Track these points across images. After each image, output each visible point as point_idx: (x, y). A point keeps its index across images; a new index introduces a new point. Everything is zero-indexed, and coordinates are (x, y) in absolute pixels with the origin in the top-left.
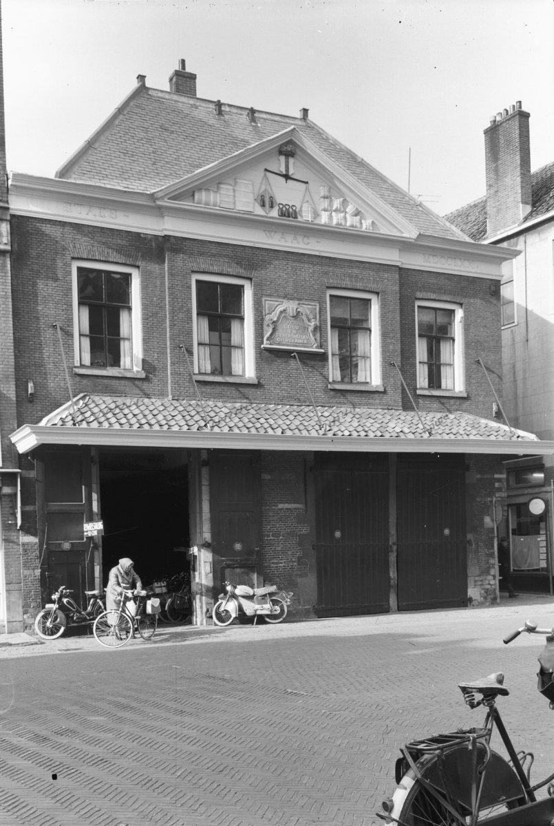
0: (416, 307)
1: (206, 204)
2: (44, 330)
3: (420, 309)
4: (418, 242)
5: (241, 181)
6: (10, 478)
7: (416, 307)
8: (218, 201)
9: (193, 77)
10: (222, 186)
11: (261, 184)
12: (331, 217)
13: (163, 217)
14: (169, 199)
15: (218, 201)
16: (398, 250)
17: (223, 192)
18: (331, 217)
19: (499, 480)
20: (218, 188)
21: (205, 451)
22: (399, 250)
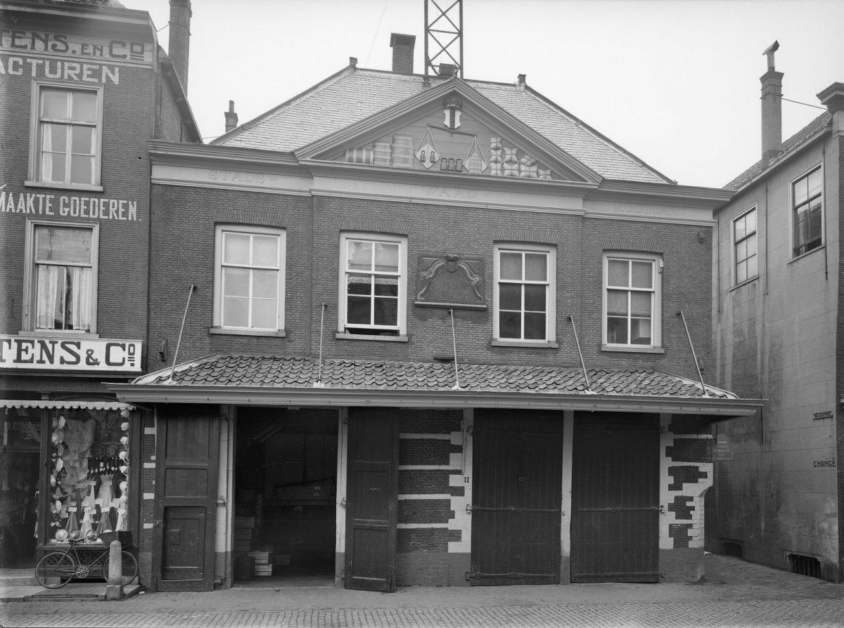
0: (605, 293)
1: (366, 163)
2: (162, 248)
3: (612, 295)
4: (601, 189)
5: (400, 137)
6: (843, 596)
7: (605, 293)
8: (372, 159)
9: (781, 75)
10: (377, 144)
11: (818, 187)
12: (503, 170)
13: (312, 178)
14: (312, 158)
15: (372, 159)
16: (581, 200)
17: (377, 149)
18: (503, 170)
19: (316, 491)
20: (374, 146)
21: (346, 411)
22: (583, 200)
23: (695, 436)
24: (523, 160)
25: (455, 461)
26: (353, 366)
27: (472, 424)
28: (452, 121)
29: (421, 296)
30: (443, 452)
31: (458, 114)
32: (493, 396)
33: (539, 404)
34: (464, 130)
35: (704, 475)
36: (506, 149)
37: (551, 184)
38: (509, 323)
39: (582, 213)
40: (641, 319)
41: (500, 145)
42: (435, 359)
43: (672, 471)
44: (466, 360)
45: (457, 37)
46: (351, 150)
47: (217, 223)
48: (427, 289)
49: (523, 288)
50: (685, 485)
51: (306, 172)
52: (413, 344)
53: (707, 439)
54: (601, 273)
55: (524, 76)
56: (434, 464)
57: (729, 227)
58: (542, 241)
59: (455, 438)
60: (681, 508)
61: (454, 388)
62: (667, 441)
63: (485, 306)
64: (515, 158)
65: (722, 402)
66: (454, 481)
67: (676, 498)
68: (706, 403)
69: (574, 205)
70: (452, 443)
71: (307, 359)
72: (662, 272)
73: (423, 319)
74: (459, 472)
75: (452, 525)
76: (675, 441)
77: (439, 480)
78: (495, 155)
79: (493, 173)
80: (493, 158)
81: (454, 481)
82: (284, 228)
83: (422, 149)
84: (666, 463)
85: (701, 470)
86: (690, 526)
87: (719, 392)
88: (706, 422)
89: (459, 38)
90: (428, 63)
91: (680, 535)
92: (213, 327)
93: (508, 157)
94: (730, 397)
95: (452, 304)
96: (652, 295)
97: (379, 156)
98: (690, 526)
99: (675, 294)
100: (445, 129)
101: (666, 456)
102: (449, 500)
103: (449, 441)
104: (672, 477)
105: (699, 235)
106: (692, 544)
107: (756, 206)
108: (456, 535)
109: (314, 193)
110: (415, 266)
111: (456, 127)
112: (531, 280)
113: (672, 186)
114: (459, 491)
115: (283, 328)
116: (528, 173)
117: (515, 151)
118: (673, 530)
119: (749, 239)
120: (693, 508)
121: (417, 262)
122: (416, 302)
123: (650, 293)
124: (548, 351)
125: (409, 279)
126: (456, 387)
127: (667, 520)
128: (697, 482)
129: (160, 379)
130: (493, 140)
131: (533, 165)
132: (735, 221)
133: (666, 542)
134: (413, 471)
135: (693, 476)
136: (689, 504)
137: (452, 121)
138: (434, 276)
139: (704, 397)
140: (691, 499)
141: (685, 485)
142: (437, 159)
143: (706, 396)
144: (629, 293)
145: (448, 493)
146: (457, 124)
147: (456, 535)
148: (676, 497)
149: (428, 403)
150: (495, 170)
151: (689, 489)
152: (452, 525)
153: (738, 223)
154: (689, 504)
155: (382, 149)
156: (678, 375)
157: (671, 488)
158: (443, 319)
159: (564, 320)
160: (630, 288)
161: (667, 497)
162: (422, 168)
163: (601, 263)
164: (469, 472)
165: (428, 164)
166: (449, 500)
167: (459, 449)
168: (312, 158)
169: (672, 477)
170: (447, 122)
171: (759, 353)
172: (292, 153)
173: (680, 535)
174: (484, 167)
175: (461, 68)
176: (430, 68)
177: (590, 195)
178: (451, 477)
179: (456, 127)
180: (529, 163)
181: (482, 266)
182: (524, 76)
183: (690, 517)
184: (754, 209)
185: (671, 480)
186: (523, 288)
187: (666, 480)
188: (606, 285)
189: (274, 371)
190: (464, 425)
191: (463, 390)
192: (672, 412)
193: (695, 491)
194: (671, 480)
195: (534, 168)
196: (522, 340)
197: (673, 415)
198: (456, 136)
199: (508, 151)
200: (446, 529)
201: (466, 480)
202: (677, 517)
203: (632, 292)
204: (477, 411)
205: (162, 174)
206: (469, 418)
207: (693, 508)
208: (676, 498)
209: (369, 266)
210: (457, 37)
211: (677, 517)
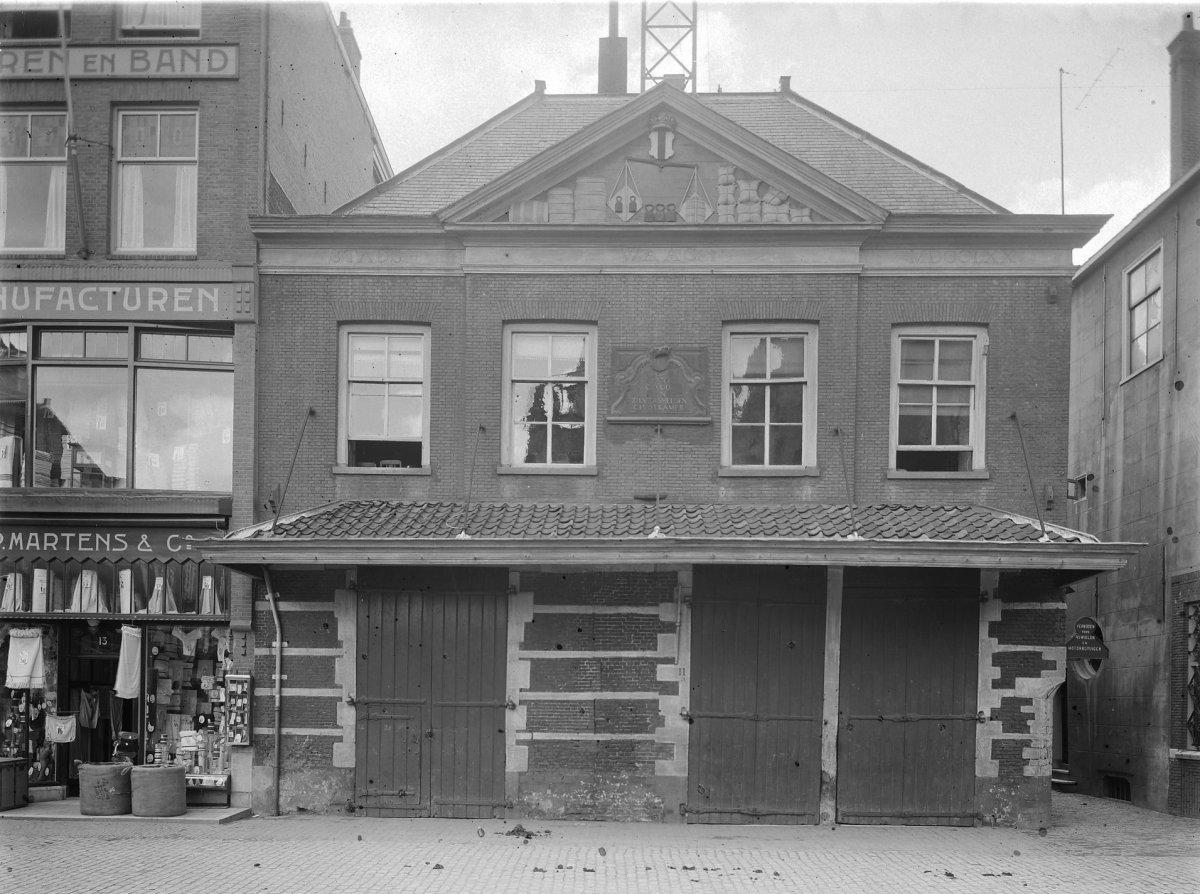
7: (895, 394)
23: (1037, 606)
24: (768, 197)
25: (665, 644)
26: (615, 513)
27: (689, 591)
28: (662, 149)
29: (616, 408)
30: (647, 632)
31: (669, 137)
32: (498, 546)
33: (631, 555)
34: (680, 160)
35: (1051, 665)
36: (739, 182)
37: (810, 229)
38: (747, 445)
39: (858, 271)
40: (955, 427)
41: (731, 178)
42: (635, 498)
43: (997, 659)
44: (681, 499)
45: (651, 27)
46: (518, 204)
47: (340, 323)
48: (625, 397)
49: (768, 390)
50: (1019, 681)
51: (457, 239)
52: (605, 478)
53: (1058, 609)
54: (888, 360)
55: (789, 78)
56: (635, 649)
57: (1120, 284)
58: (796, 317)
59: (666, 613)
60: (1013, 715)
61: (651, 536)
62: (992, 613)
63: (709, 419)
64: (754, 195)
65: (1074, 548)
66: (664, 673)
67: (1005, 701)
68: (1045, 551)
69: (847, 258)
70: (662, 619)
71: (458, 504)
72: (990, 354)
73: (618, 440)
74: (669, 661)
75: (658, 736)
76: (1004, 613)
77: (644, 675)
78: (725, 193)
79: (722, 220)
80: (721, 199)
81: (664, 673)
82: (428, 324)
83: (618, 194)
84: (989, 646)
85: (1046, 657)
86: (1027, 743)
87: (1068, 534)
88: (1058, 581)
89: (691, 33)
90: (645, 75)
91: (1009, 756)
92: (721, 467)
93: (744, 196)
94: (1084, 541)
95: (661, 418)
96: (972, 391)
97: (559, 210)
98: (1027, 743)
99: (1008, 386)
100: (651, 161)
101: (990, 636)
102: (656, 702)
103: (657, 616)
104: (998, 669)
105: (1047, 291)
106: (1029, 771)
107: (1162, 245)
108: (665, 751)
109: (467, 270)
110: (609, 365)
111: (667, 157)
112: (946, 379)
113: (1004, 216)
114: (670, 688)
115: (815, 464)
116: (774, 216)
117: (754, 185)
118: (999, 750)
119: (1143, 296)
120: (1032, 716)
121: (614, 359)
122: (609, 418)
123: (969, 387)
124: (803, 480)
125: (601, 385)
126: (655, 534)
127: (988, 734)
128: (1039, 676)
129: (259, 533)
130: (722, 171)
131: (782, 202)
132: (1130, 274)
133: (987, 766)
134: (626, 659)
135: (1033, 666)
136: (1025, 709)
137: (662, 149)
138: (633, 380)
139: (1041, 540)
140: (1028, 701)
141: (1019, 681)
142: (638, 207)
143: (1044, 539)
144: (935, 390)
145: (655, 691)
146: (669, 153)
147: (665, 751)
148: (1004, 699)
149: (504, 559)
150: (725, 217)
151: (1025, 686)
152: (658, 736)
153: (1134, 276)
154: (1025, 709)
155: (561, 198)
156: (1012, 511)
157: (996, 684)
158: (647, 439)
159: (830, 433)
160: (936, 381)
161: (988, 700)
162: (617, 222)
163: (888, 346)
164: (685, 659)
165: (626, 216)
166: (656, 702)
167: (670, 628)
168: (462, 220)
169: (998, 669)
170: (654, 152)
171: (1162, 477)
172: (435, 216)
173: (1009, 756)
174: (709, 213)
175: (693, 76)
176: (195, 56)
177: (872, 240)
178: (660, 667)
179: (667, 157)
180: (777, 200)
181: (706, 361)
182: (789, 78)
183: (1026, 729)
184: (1159, 250)
185: (996, 673)
186: (768, 390)
187: (988, 672)
188: (897, 378)
189: (409, 521)
190: (678, 594)
191: (827, 539)
192: (694, 561)
193: (1038, 689)
194: (996, 673)
195: (785, 208)
196: (767, 466)
197: (694, 565)
198: (667, 169)
199: (743, 185)
200: (652, 742)
201: (681, 672)
202: (1005, 730)
203: (938, 387)
204: (699, 569)
205: (279, 261)
206: (685, 578)
207: (1032, 716)
208: (1005, 701)
209: (764, 376)
210: (651, 27)
211: (1005, 730)
